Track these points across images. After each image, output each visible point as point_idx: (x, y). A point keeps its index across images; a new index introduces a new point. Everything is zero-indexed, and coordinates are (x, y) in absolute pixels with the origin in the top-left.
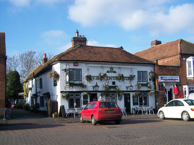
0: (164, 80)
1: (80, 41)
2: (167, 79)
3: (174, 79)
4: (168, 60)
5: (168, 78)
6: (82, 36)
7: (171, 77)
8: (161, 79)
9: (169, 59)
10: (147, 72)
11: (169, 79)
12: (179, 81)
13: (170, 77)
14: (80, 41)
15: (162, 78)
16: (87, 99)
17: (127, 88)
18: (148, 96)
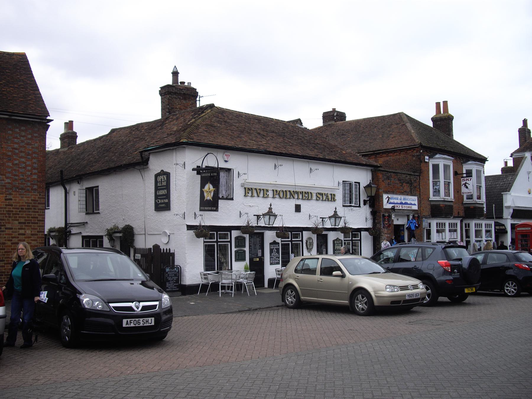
0: (393, 205)
1: (178, 96)
2: (398, 204)
3: (409, 202)
4: (388, 158)
5: (399, 201)
6: (186, 84)
7: (404, 199)
8: (388, 202)
9: (390, 156)
10: (359, 183)
11: (401, 203)
12: (415, 208)
13: (402, 197)
14: (178, 96)
15: (388, 200)
16: (245, 246)
17: (258, 219)
18: (360, 240)
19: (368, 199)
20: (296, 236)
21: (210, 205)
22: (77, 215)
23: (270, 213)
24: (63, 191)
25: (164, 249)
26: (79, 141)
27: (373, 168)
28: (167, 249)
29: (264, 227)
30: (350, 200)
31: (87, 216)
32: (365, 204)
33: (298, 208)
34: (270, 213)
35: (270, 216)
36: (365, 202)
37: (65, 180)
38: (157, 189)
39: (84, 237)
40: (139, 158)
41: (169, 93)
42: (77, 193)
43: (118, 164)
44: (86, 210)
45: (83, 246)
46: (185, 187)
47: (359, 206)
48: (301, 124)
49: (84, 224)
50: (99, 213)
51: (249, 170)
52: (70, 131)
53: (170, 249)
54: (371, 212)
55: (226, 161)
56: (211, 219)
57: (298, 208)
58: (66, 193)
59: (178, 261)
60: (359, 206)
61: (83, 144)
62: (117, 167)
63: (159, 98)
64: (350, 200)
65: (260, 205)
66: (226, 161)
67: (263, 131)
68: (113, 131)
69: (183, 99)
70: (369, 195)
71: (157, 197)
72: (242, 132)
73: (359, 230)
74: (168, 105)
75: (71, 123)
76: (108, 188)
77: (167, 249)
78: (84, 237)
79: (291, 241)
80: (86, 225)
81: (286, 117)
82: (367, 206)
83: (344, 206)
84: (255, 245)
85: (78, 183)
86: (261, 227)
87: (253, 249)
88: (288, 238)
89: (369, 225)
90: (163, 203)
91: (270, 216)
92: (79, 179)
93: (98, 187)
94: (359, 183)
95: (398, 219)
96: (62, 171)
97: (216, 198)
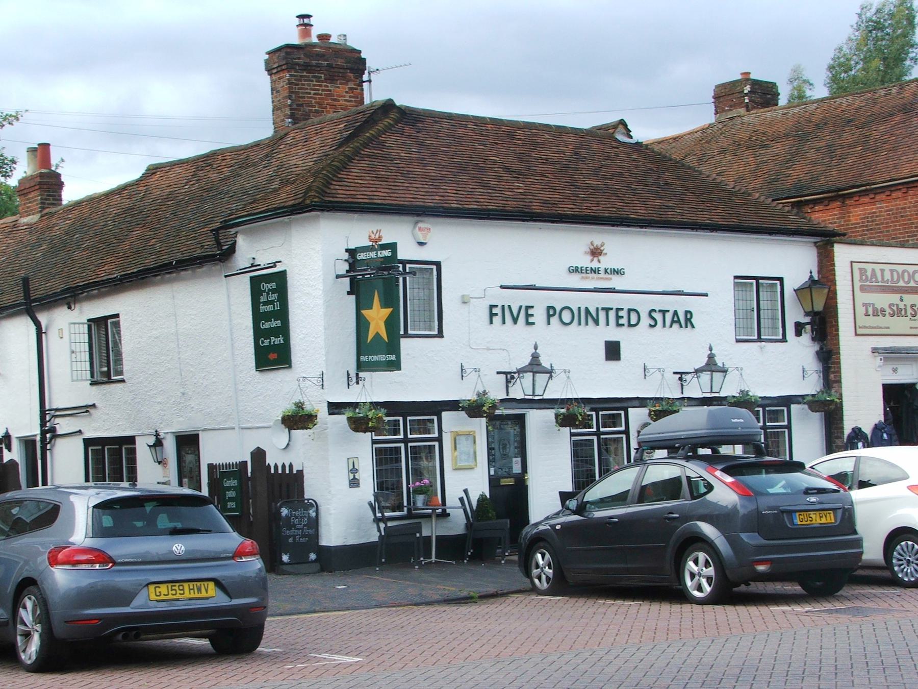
4: (873, 208)
10: (781, 280)
14: (313, 69)
18: (789, 427)
19: (807, 319)
20: (613, 420)
21: (377, 351)
22: (70, 384)
23: (535, 366)
24: (33, 328)
25: (276, 466)
26: (70, 194)
27: (818, 239)
28: (284, 466)
29: (523, 401)
30: (757, 326)
31: (95, 388)
32: (798, 333)
33: (613, 351)
34: (535, 366)
35: (534, 373)
36: (799, 329)
37: (35, 301)
38: (258, 317)
39: (88, 442)
40: (209, 242)
41: (290, 66)
42: (67, 326)
43: (165, 259)
44: (92, 376)
45: (87, 480)
46: (319, 316)
47: (784, 340)
48: (628, 133)
49: (87, 409)
50: (123, 381)
51: (474, 261)
52: (43, 171)
53: (291, 466)
54: (817, 353)
55: (421, 244)
56: (381, 388)
57: (613, 351)
58: (40, 333)
59: (311, 491)
60: (784, 340)
61: (78, 204)
62: (160, 266)
63: (265, 81)
64: (757, 326)
65: (514, 345)
66: (421, 244)
67: (521, 160)
68: (153, 170)
69: (326, 80)
70: (809, 309)
71: (258, 333)
72: (462, 168)
73: (787, 401)
74: (290, 97)
75: (45, 147)
76: (140, 313)
77: (284, 466)
78: (88, 442)
79: (598, 434)
80: (92, 411)
81: (582, 115)
82: (806, 338)
83: (738, 341)
84: (504, 447)
85: (69, 308)
86: (514, 400)
87: (498, 455)
88: (590, 427)
89: (811, 386)
90: (273, 352)
91: (534, 373)
92: (70, 296)
93: (117, 316)
94: (781, 280)
95: (895, 370)
96: (26, 281)
97: (395, 332)
